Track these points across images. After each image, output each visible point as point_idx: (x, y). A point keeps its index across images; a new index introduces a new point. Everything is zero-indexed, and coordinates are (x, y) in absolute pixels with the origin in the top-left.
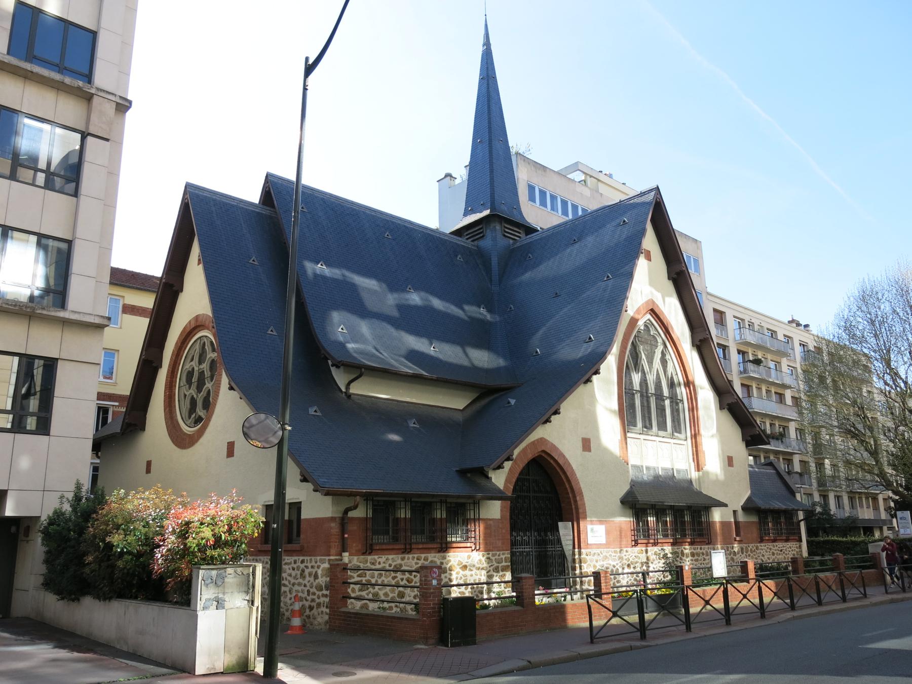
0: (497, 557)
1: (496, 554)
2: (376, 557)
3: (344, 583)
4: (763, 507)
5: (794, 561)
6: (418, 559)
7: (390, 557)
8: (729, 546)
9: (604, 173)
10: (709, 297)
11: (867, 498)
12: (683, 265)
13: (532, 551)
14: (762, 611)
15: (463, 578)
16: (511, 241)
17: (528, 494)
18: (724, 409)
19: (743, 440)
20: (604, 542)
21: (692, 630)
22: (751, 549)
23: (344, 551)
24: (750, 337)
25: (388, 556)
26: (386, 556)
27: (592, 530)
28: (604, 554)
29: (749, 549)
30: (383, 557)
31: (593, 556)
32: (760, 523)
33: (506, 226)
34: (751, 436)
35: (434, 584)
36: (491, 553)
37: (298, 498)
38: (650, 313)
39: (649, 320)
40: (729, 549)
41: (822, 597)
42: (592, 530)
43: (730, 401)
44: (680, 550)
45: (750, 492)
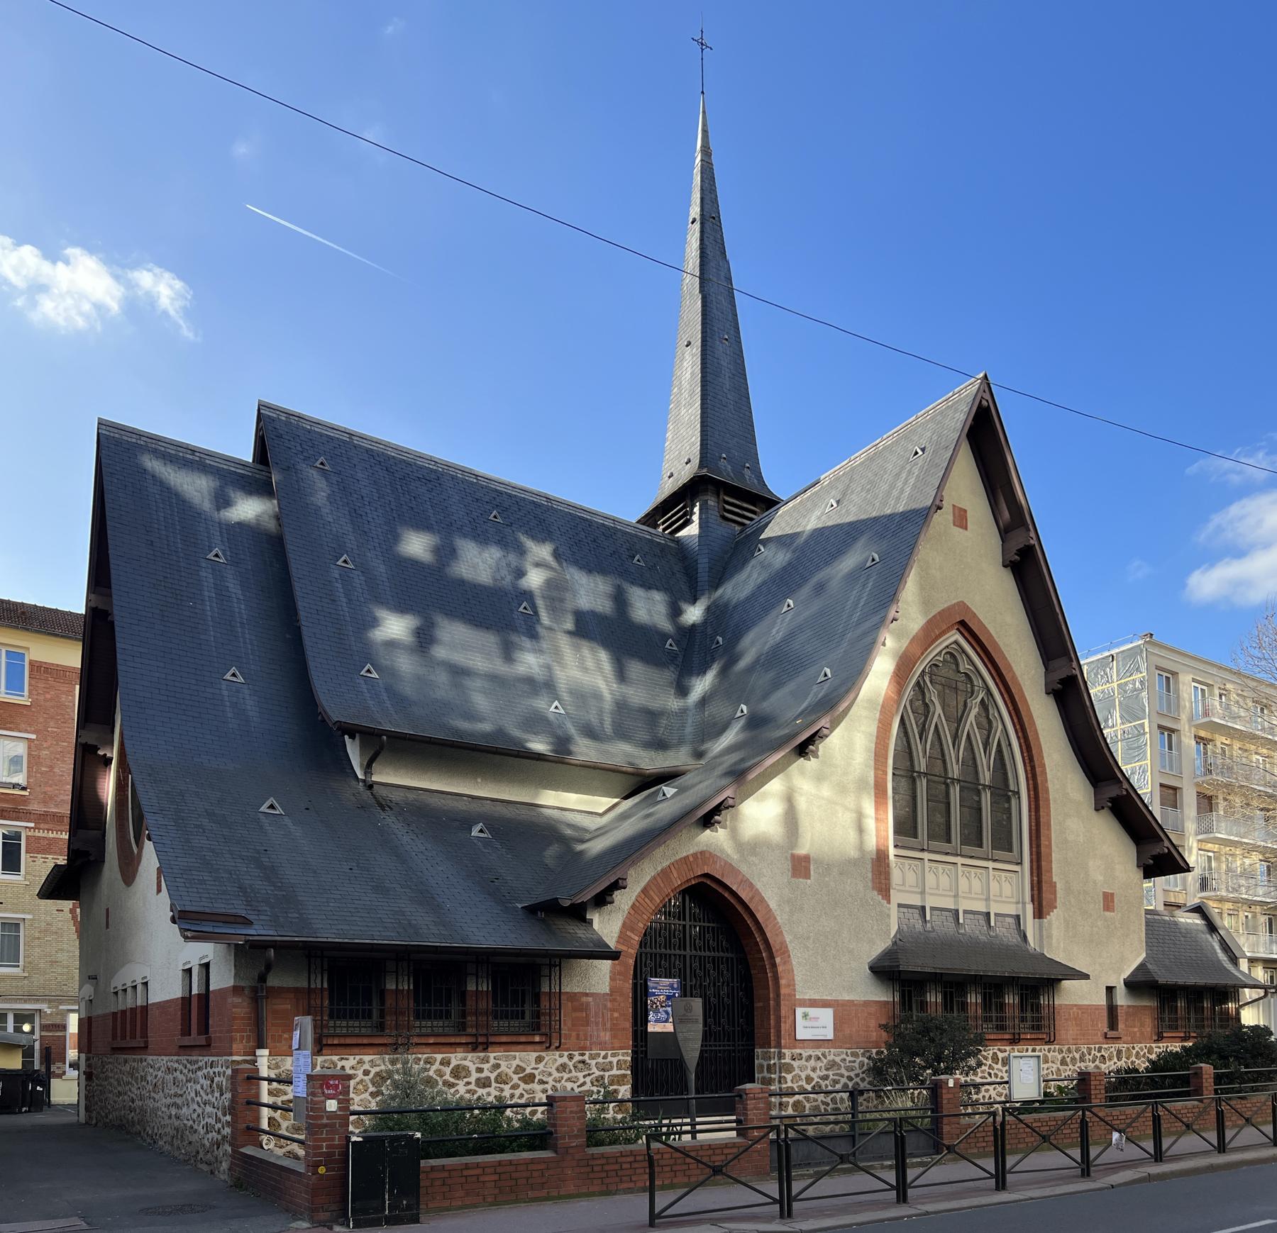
0: (600, 1060)
1: (600, 1054)
2: (335, 1058)
3: (249, 1103)
4: (1161, 980)
5: (1084, 1079)
6: (442, 1063)
7: (367, 1058)
8: (1093, 1046)
12: (1032, 534)
13: (734, 1051)
14: (1085, 1166)
15: (526, 1096)
16: (738, 528)
17: (682, 952)
18: (1103, 808)
19: (1138, 866)
20: (830, 1036)
21: (1092, 1174)
22: (1138, 1052)
23: (261, 1046)
25: (361, 1057)
26: (358, 1057)
27: (805, 1016)
28: (831, 1058)
29: (1134, 1052)
30: (352, 1057)
31: (810, 1056)
32: (1161, 1008)
34: (1154, 857)
36: (587, 1053)
38: (958, 629)
39: (956, 642)
40: (1093, 1052)
41: (1165, 1146)
42: (805, 1016)
43: (1113, 792)
44: (991, 1052)
45: (1144, 955)
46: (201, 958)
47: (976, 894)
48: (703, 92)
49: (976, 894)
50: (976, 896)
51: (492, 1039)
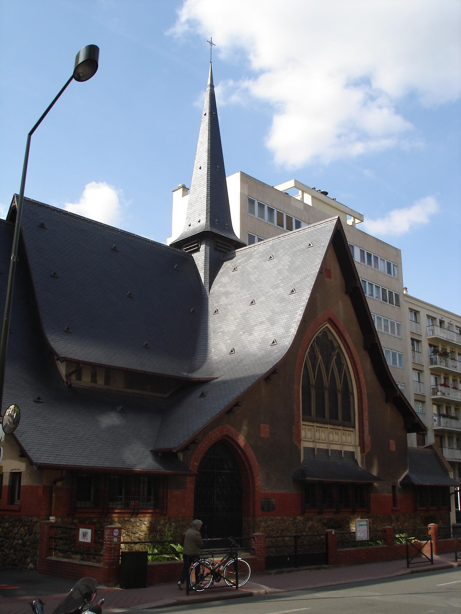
9: (317, 189)
10: (406, 299)
11: (147, 546)
24: (440, 333)
33: (218, 241)
35: (115, 541)
37: (19, 469)
41: (458, 556)
46: (12, 470)
47: (308, 438)
48: (211, 62)
49: (322, 440)
50: (322, 441)
51: (140, 511)
